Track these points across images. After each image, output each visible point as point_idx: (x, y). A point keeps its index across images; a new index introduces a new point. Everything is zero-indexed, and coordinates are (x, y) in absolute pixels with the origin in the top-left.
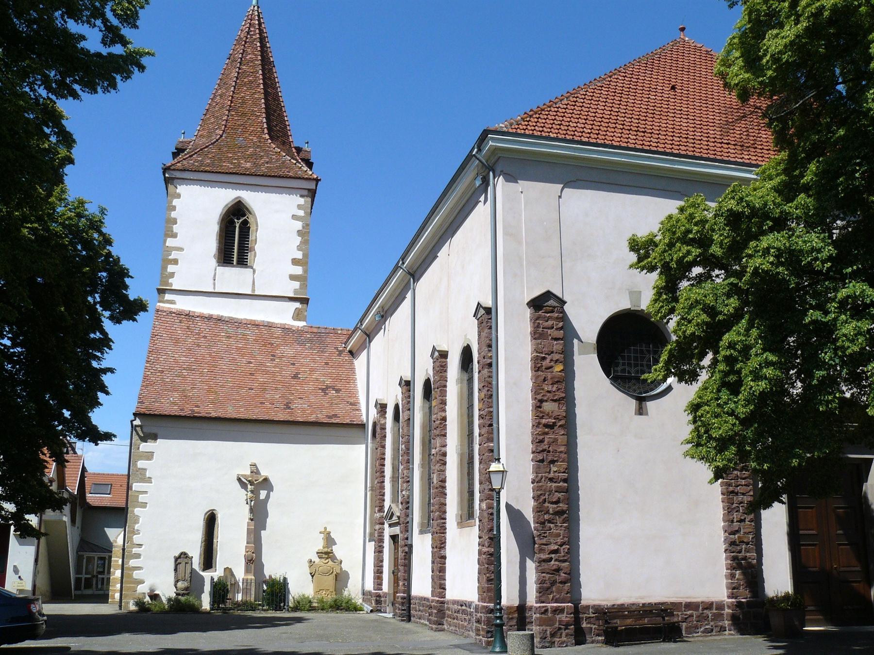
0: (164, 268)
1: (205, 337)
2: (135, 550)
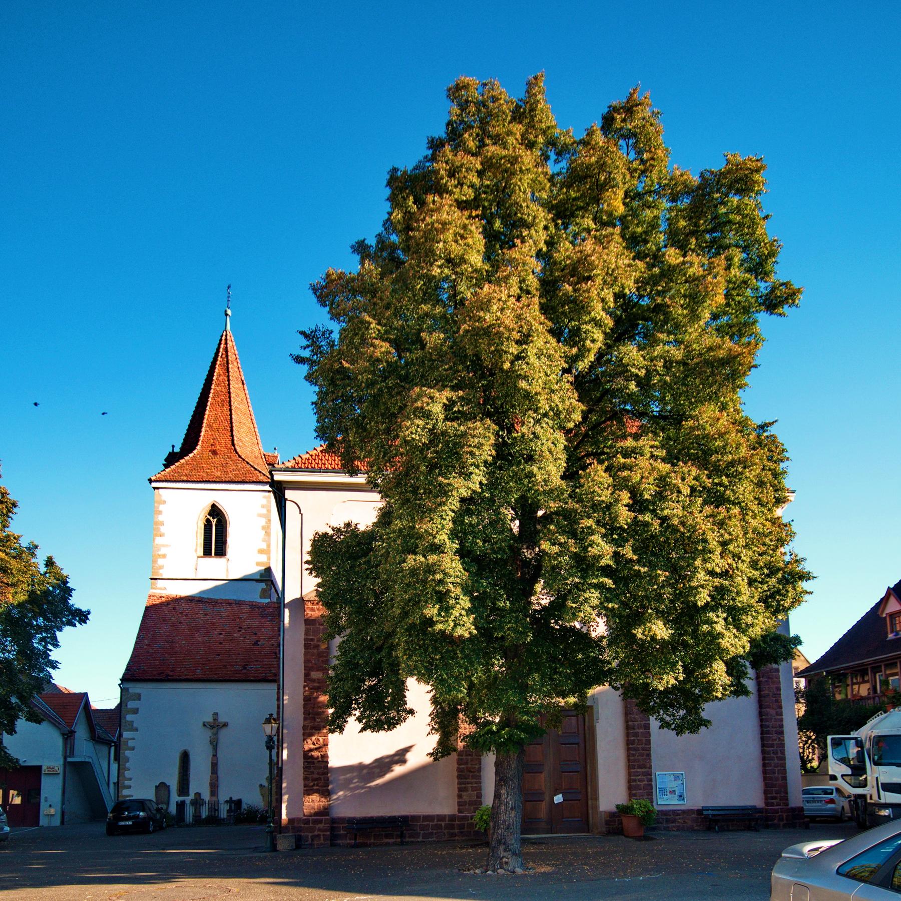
0: (155, 561)
1: (186, 615)
2: (127, 783)
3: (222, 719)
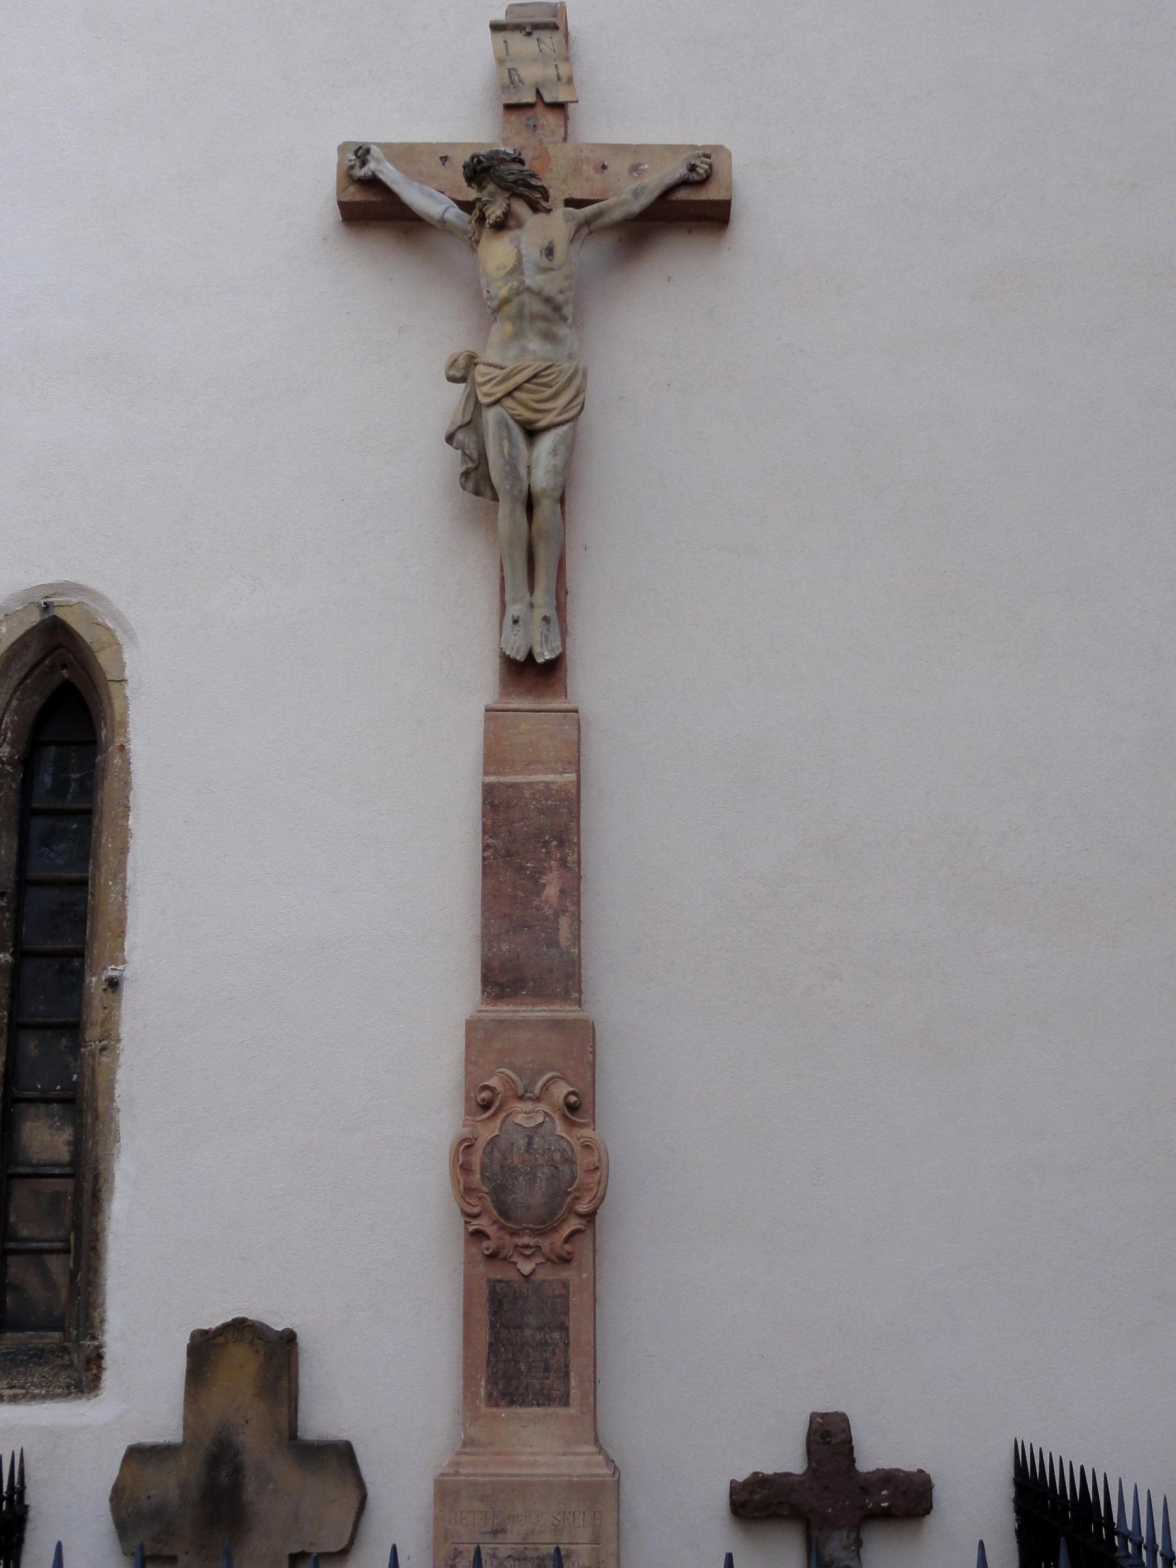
3: (636, 106)
